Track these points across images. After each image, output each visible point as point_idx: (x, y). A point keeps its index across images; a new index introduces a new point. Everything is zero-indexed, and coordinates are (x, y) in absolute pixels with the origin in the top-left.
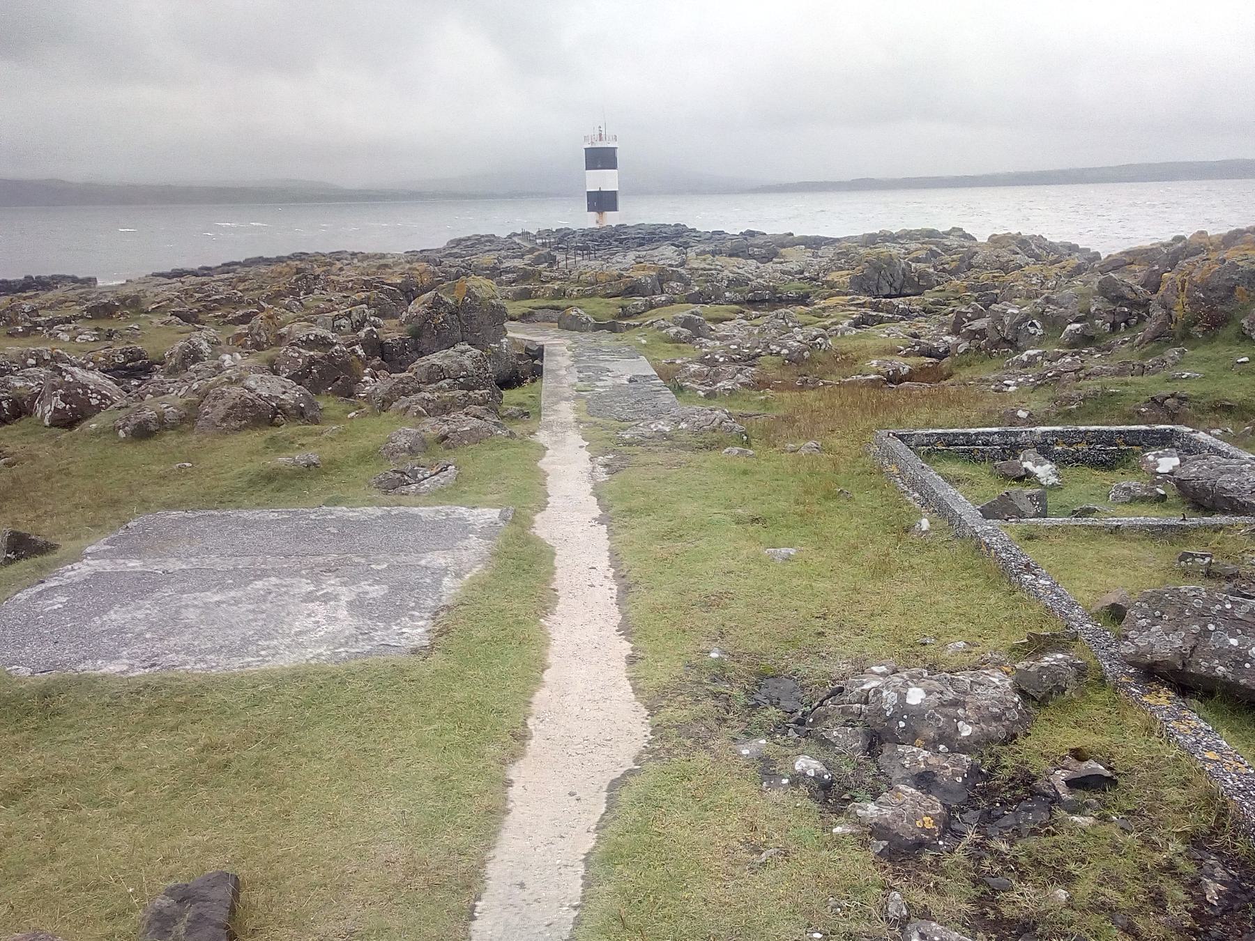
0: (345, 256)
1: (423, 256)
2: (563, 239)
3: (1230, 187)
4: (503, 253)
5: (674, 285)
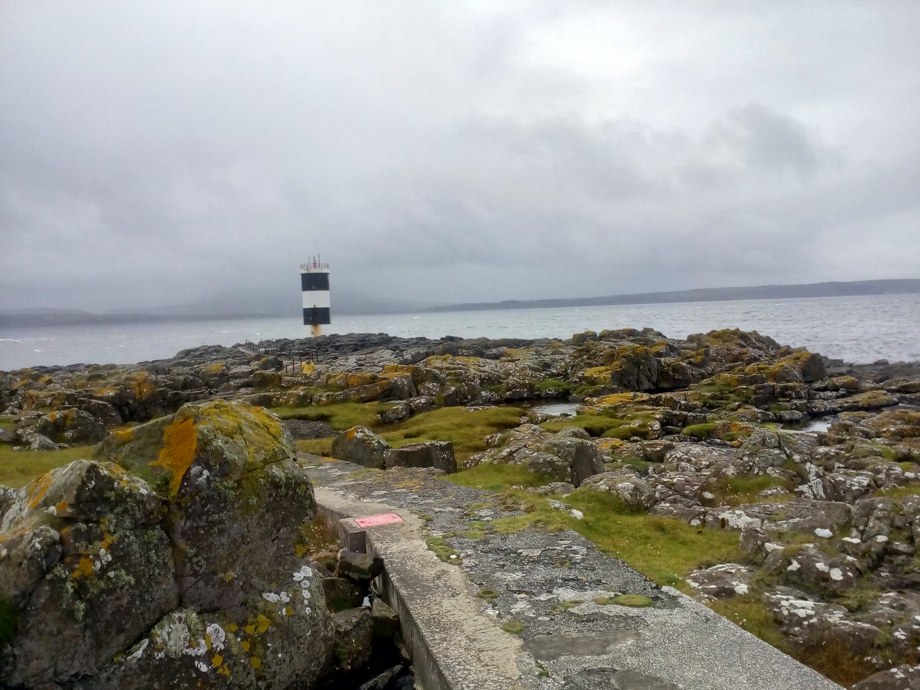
0: (82, 367)
1: (155, 367)
2: (284, 347)
3: (698, 308)
4: (230, 360)
5: (431, 385)
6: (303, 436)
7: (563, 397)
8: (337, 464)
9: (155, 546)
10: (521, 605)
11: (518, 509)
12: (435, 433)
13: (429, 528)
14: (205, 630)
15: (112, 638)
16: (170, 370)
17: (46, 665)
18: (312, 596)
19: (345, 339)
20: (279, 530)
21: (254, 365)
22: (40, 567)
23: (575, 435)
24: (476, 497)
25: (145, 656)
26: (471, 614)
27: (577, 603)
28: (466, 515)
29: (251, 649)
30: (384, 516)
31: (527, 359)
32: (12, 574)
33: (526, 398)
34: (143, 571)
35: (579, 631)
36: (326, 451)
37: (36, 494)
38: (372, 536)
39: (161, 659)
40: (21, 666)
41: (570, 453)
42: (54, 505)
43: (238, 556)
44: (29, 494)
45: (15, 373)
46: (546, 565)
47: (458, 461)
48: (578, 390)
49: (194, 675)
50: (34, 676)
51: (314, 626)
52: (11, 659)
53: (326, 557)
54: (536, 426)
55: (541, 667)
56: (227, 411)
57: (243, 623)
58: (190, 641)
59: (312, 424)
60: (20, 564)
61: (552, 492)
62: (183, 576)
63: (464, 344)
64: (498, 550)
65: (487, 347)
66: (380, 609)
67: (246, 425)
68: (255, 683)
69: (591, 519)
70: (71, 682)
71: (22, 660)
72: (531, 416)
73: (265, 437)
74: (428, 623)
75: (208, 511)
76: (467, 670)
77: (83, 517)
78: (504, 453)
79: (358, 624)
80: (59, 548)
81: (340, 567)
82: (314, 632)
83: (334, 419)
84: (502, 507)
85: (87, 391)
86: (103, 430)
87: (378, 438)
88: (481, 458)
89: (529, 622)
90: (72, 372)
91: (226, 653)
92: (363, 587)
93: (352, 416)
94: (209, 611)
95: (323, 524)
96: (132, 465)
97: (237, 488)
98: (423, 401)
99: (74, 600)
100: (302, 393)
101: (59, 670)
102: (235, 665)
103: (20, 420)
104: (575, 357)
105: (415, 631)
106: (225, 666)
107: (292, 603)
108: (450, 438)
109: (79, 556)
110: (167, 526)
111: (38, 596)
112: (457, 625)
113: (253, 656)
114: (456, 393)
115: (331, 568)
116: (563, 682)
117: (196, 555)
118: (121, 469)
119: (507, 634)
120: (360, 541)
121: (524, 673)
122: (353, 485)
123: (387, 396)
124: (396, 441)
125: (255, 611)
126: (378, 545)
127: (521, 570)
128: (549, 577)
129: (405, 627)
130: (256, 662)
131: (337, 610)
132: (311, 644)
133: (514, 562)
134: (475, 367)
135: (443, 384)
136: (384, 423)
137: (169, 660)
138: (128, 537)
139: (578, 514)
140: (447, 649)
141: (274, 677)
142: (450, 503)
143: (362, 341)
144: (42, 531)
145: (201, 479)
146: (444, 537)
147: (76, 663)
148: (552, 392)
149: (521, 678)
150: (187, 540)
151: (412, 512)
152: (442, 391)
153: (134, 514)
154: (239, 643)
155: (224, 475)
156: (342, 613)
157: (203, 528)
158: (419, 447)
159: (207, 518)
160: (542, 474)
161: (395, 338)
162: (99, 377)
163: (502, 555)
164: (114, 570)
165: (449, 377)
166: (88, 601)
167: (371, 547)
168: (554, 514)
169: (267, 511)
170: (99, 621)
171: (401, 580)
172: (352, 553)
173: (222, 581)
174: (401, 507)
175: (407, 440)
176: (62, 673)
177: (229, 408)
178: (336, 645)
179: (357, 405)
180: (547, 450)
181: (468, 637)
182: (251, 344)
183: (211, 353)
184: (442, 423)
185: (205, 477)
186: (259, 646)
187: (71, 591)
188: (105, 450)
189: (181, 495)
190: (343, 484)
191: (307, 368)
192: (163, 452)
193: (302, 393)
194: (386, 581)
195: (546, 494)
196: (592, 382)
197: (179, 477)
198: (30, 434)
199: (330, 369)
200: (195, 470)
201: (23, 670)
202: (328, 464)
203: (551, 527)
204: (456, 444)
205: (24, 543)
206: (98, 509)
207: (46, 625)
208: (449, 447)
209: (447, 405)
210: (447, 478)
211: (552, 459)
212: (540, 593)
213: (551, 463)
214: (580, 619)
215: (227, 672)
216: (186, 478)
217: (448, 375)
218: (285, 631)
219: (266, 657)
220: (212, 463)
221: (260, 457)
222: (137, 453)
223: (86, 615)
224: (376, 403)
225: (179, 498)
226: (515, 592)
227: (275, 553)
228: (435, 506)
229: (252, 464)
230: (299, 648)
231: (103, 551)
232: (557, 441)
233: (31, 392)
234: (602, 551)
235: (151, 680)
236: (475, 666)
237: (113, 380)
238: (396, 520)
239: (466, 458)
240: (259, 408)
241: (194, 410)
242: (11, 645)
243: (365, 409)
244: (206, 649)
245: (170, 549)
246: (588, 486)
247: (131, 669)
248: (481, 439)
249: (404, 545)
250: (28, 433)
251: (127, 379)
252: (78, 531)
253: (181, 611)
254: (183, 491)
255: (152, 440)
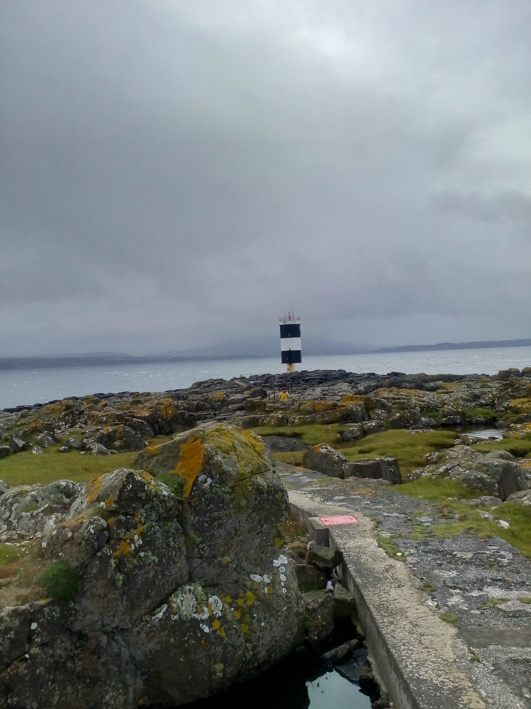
1: (176, 395)
2: (267, 381)
4: (229, 390)
5: (379, 412)
6: (281, 449)
7: (490, 423)
8: (307, 472)
9: (173, 534)
10: (455, 600)
11: (453, 518)
12: (383, 450)
13: (379, 529)
14: (208, 600)
15: (142, 602)
16: (187, 397)
17: (96, 618)
18: (287, 579)
19: (312, 374)
20: (262, 526)
21: (246, 394)
22: (93, 546)
23: (502, 457)
24: (418, 506)
25: (164, 617)
26: (414, 604)
27: (504, 600)
28: (409, 520)
29: (241, 617)
30: (345, 518)
31: (459, 392)
32: (75, 550)
33: (460, 423)
34: (164, 553)
35: (506, 625)
36: (298, 462)
37: (92, 493)
38: (334, 533)
39: (176, 620)
40: (80, 617)
41: (497, 472)
42: (104, 501)
43: (232, 545)
44: (87, 492)
45: (83, 399)
46: (477, 566)
47: (403, 474)
48: (504, 418)
49: (199, 635)
50: (89, 626)
51: (289, 603)
52: (73, 612)
53: (298, 547)
54: (468, 447)
55: (473, 653)
56: (225, 434)
57: (235, 597)
58: (197, 608)
59: (288, 440)
60: (80, 544)
61: (482, 504)
62: (192, 558)
63: (406, 379)
64: (436, 551)
65: (426, 381)
66: (340, 593)
67: (238, 444)
68: (244, 644)
69: (515, 528)
70: (113, 632)
71: (81, 613)
72: (463, 439)
73: (251, 454)
74: (378, 608)
75: (211, 509)
76: (411, 650)
77: (123, 511)
78: (441, 470)
79: (322, 604)
80: (106, 533)
81: (309, 557)
82: (289, 608)
83: (304, 437)
84: (440, 515)
85: (130, 412)
86: (141, 441)
87: (338, 453)
88: (421, 472)
89: (463, 614)
90: (121, 398)
91: (223, 619)
92: (328, 574)
93: (318, 435)
94: (211, 586)
95: (296, 520)
96: (157, 473)
97: (232, 493)
98: (374, 424)
99: (116, 572)
100: (280, 416)
101: (105, 624)
102: (229, 629)
103: (85, 433)
104: (500, 390)
105: (368, 613)
106: (222, 629)
107: (273, 584)
108: (395, 456)
109: (120, 539)
110: (182, 521)
111: (92, 568)
112: (402, 612)
113: (243, 623)
114: (400, 418)
115: (302, 556)
116: (492, 668)
117: (202, 543)
118: (150, 475)
119: (444, 623)
120: (325, 536)
121: (458, 657)
122: (319, 490)
123: (345, 420)
124: (352, 456)
125: (244, 589)
126: (338, 540)
127: (456, 569)
128: (480, 577)
129: (360, 608)
130: (245, 628)
131: (307, 590)
132: (287, 617)
133: (450, 562)
134: (416, 398)
135: (389, 411)
136: (342, 441)
137: (181, 622)
138: (154, 527)
139: (505, 524)
140: (394, 631)
141: (258, 641)
142: (397, 510)
143: (325, 376)
144: (95, 520)
145: (205, 485)
146: (392, 537)
147: (117, 619)
148: (481, 419)
149: (456, 661)
150: (196, 531)
151: (365, 515)
152: (389, 416)
153: (159, 510)
154: (232, 612)
155: (222, 482)
156: (311, 593)
157: (207, 522)
158: (370, 462)
159: (210, 515)
160: (473, 488)
161: (351, 373)
162: (139, 402)
163: (439, 555)
164: (144, 551)
165: (394, 406)
166: (125, 573)
167: (333, 541)
168: (484, 523)
169: (254, 511)
170: (133, 589)
171: (357, 571)
172: (318, 546)
173: (220, 563)
174: (357, 510)
175: (361, 455)
176: (107, 625)
177: (226, 431)
178: (306, 619)
179: (322, 426)
180: (478, 469)
181: (411, 622)
182: (244, 378)
183: (216, 385)
184: (389, 442)
185: (208, 483)
186: (247, 615)
187: (114, 565)
188: (140, 461)
189: (191, 497)
190: (311, 489)
191: (283, 396)
192: (180, 464)
193: (280, 416)
194: (345, 570)
195: (477, 506)
196: (516, 411)
197: (190, 483)
198: (91, 443)
199: (301, 398)
200: (202, 478)
201: (82, 621)
202: (300, 471)
203: (481, 534)
204: (401, 460)
205: (83, 529)
206: (133, 505)
207: (97, 590)
208: (395, 463)
209: (394, 428)
210: (393, 488)
211: (481, 477)
212: (472, 590)
213: (481, 480)
214: (507, 614)
215: (224, 634)
216: (195, 484)
217: (394, 404)
218: (267, 605)
219: (252, 625)
220: (214, 473)
221: (248, 470)
222: (161, 464)
223: (124, 584)
224: (336, 425)
225: (190, 499)
226: (451, 587)
227: (260, 544)
228: (384, 511)
229: (243, 475)
230: (277, 619)
231: (136, 537)
232: (486, 462)
233: (93, 412)
234: (526, 557)
235: (169, 635)
236: (418, 648)
237: (148, 404)
238: (352, 521)
239: (409, 471)
240: (247, 431)
241: (201, 433)
242: (74, 602)
243: (327, 430)
244: (208, 615)
245: (184, 537)
246: (513, 501)
247: (154, 626)
248: (421, 457)
249: (359, 542)
250: (90, 442)
251: (158, 404)
252: (120, 521)
253: (191, 585)
254: (193, 493)
255: (172, 455)
